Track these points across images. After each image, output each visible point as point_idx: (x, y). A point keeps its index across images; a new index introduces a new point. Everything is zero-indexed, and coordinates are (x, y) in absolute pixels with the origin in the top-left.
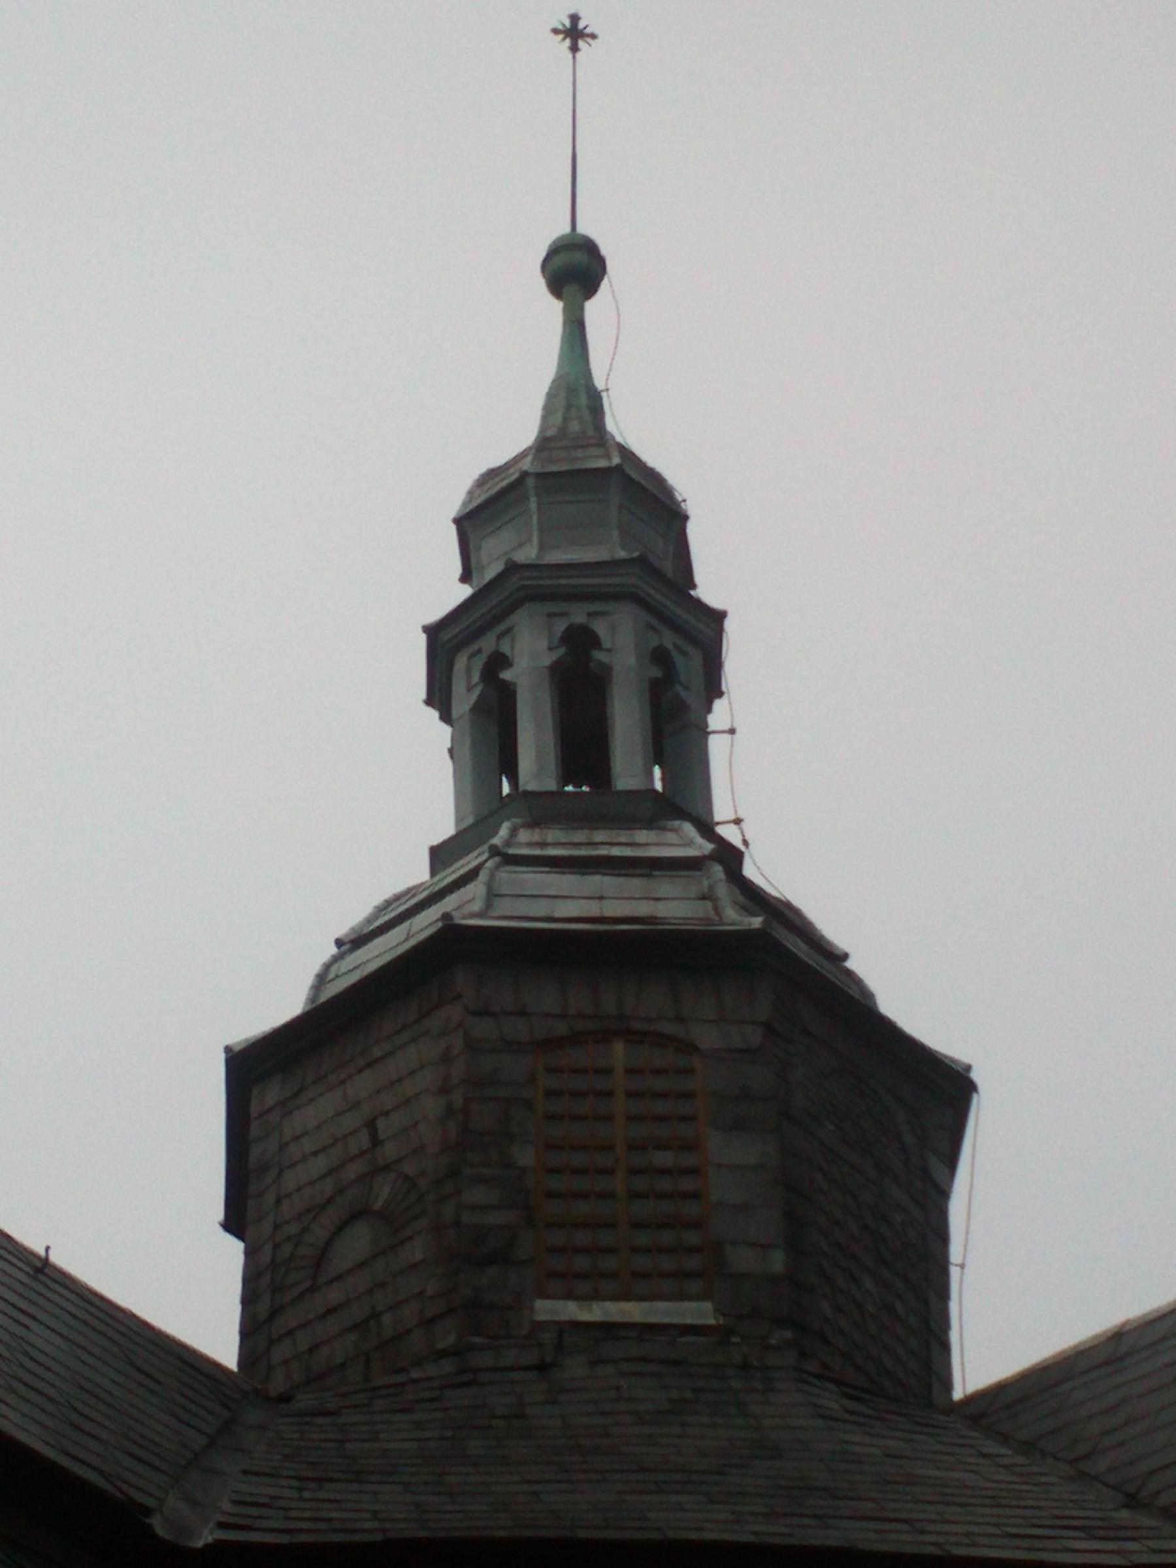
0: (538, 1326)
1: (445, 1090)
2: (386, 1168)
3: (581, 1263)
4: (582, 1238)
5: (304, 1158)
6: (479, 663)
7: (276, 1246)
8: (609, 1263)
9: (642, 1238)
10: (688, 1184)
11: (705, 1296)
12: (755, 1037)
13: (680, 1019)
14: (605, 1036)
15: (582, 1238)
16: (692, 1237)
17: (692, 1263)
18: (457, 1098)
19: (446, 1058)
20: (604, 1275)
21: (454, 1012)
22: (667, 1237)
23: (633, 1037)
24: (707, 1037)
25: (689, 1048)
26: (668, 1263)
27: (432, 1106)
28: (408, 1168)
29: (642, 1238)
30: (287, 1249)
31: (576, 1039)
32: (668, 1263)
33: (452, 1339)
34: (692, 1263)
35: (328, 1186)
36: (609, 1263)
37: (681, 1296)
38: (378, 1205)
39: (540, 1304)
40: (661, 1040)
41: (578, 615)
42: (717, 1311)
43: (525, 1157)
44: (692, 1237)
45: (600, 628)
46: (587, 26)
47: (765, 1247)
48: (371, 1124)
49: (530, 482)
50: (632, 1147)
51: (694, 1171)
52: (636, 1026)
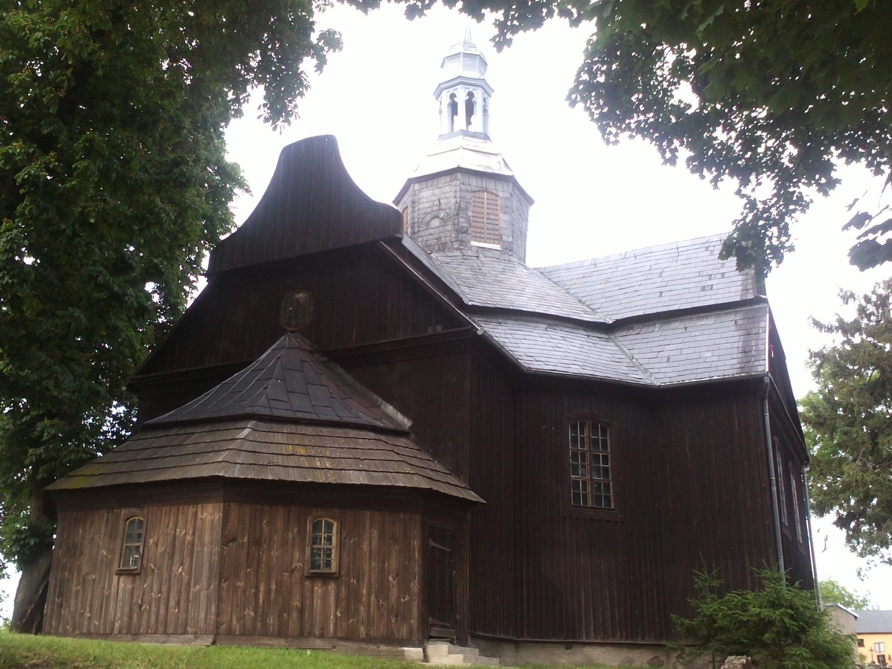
0: (472, 246)
1: (455, 197)
2: (443, 210)
3: (478, 235)
4: (478, 230)
5: (424, 203)
6: (449, 94)
7: (418, 219)
8: (482, 235)
9: (488, 232)
10: (496, 222)
11: (499, 244)
12: (509, 195)
13: (496, 190)
14: (483, 191)
15: (478, 230)
16: (496, 233)
17: (496, 237)
18: (458, 200)
19: (456, 191)
20: (482, 238)
21: (458, 183)
22: (492, 232)
23: (488, 192)
24: (501, 194)
25: (497, 196)
26: (492, 237)
27: (453, 201)
28: (447, 211)
29: (488, 232)
30: (421, 220)
31: (478, 191)
32: (492, 237)
33: (457, 246)
34: (496, 237)
35: (430, 210)
36: (482, 235)
37: (494, 243)
38: (441, 216)
39: (472, 242)
40: (493, 194)
41: (471, 89)
42: (501, 247)
43: (470, 214)
44: (496, 233)
45: (474, 92)
46: (817, 324)
47: (509, 236)
48: (439, 200)
49: (462, 54)
50: (487, 214)
51: (498, 220)
52: (489, 190)
